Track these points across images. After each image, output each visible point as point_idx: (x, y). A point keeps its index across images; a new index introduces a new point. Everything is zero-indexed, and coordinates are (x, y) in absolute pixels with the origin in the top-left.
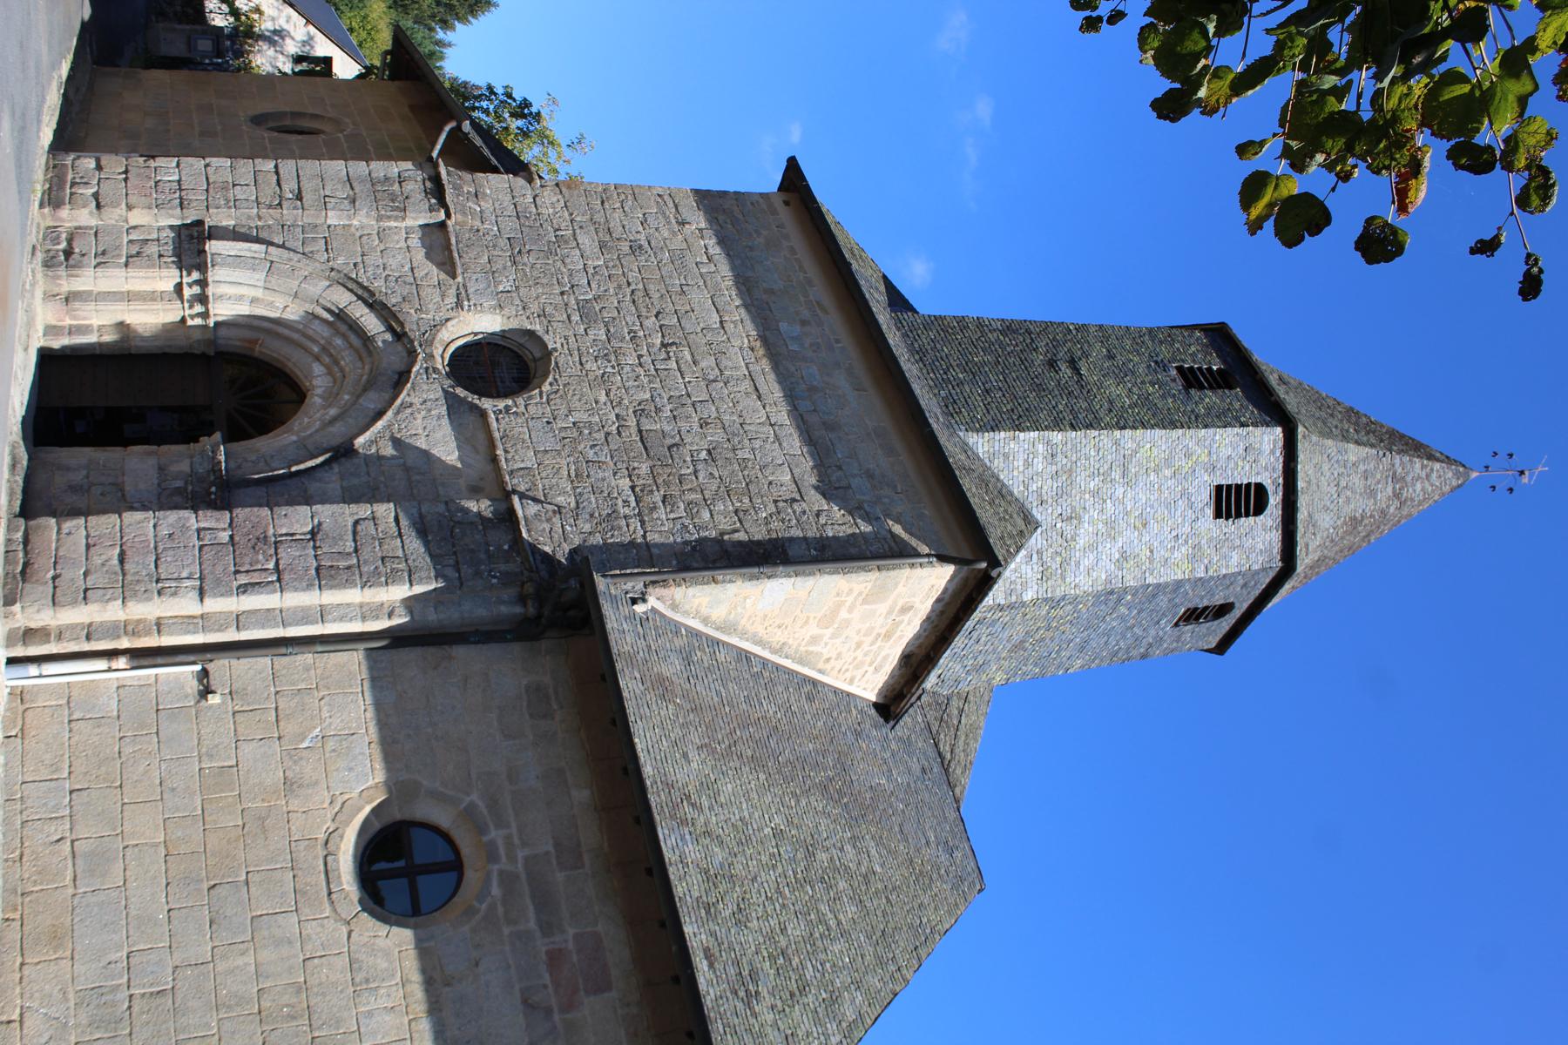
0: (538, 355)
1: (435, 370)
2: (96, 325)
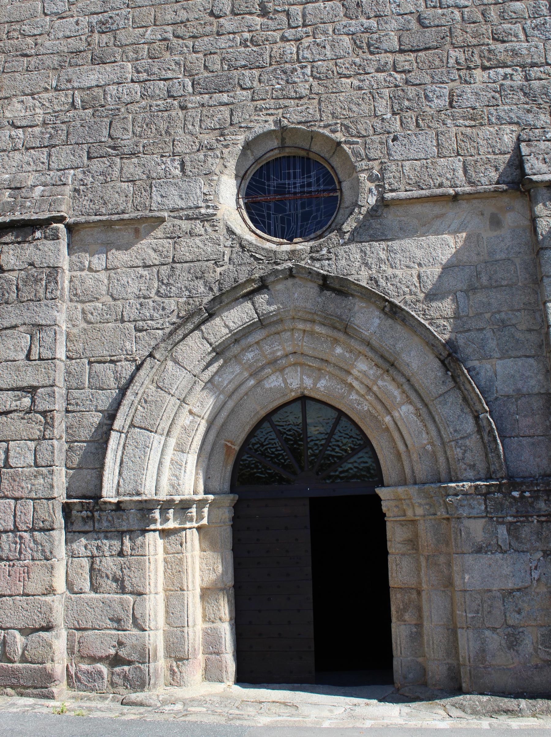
0: (275, 143)
1: (312, 250)
2: (210, 624)
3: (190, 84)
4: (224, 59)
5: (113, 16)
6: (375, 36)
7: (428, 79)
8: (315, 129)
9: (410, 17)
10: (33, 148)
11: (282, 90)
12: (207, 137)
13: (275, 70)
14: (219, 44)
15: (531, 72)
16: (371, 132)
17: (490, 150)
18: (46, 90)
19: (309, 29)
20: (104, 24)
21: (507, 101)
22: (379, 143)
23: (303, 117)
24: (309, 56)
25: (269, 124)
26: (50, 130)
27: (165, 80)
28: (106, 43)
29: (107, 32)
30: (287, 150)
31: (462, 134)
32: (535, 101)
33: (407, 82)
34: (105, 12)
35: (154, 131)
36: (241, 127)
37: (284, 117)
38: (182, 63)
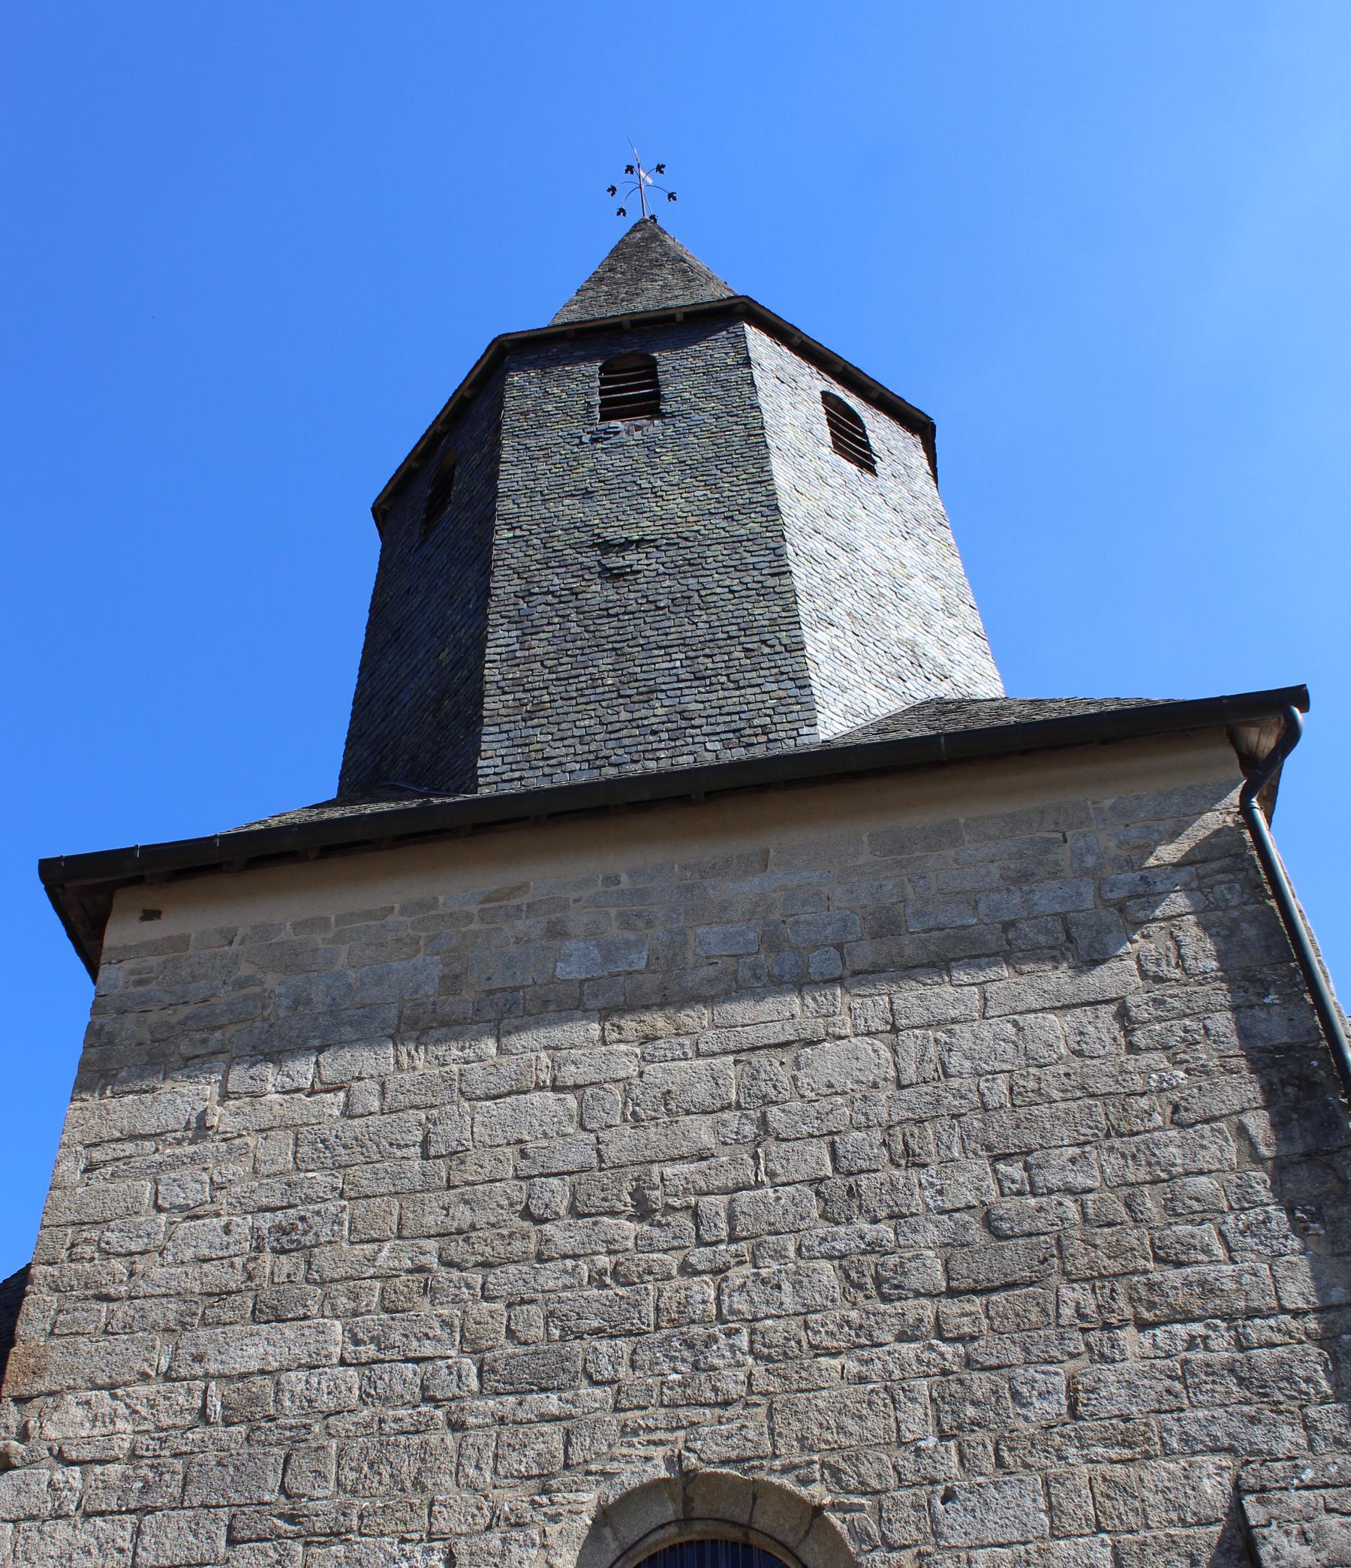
0: (670, 1511)
3: (474, 1369)
4: (552, 1314)
5: (308, 1215)
6: (892, 1260)
7: (1016, 1355)
8: (761, 1475)
9: (967, 1218)
10: (101, 1514)
11: (683, 1385)
12: (509, 1494)
13: (668, 1339)
14: (541, 1280)
15: (1249, 1330)
16: (893, 1481)
17: (1174, 1516)
18: (145, 1377)
19: (743, 1247)
20: (285, 1233)
21: (1201, 1398)
22: (913, 1506)
23: (733, 1449)
24: (744, 1307)
25: (655, 1466)
26: (145, 1471)
27: (417, 1361)
28: (289, 1276)
29: (292, 1250)
30: (698, 1526)
31: (1105, 1479)
32: (1266, 1395)
33: (969, 1363)
34: (290, 1206)
35: (386, 1479)
36: (588, 1473)
37: (689, 1450)
38: (457, 1322)
